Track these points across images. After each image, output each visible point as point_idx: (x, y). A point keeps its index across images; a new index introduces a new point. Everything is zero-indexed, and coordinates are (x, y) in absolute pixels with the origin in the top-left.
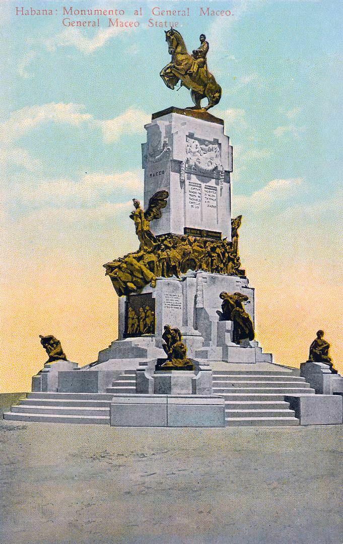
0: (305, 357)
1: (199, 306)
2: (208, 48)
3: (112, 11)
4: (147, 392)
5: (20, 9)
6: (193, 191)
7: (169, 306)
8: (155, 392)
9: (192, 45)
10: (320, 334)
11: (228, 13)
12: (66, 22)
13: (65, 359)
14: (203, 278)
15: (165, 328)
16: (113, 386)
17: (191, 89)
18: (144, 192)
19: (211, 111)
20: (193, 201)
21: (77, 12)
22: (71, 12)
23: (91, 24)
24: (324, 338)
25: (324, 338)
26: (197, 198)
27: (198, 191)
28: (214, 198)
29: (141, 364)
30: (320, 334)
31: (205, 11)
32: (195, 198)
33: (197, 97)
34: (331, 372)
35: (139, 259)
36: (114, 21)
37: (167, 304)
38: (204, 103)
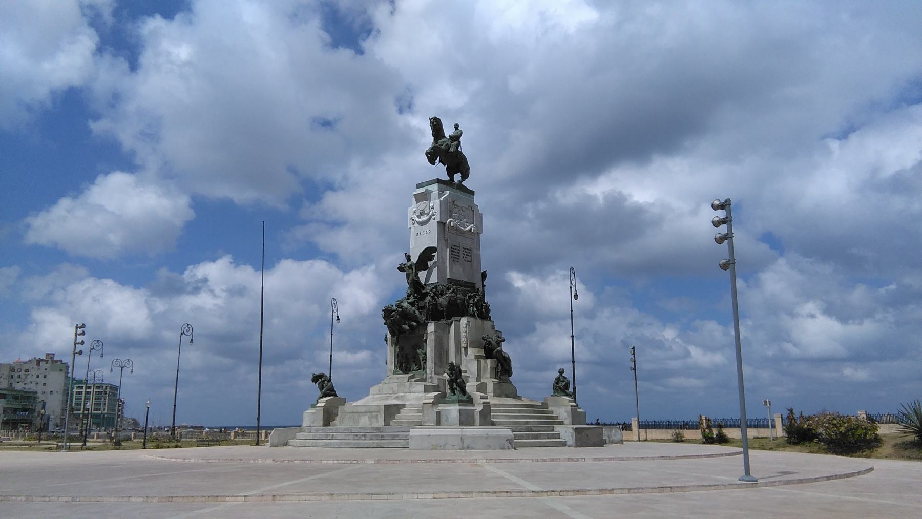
2: (462, 133)
9: (448, 131)
13: (335, 395)
15: (455, 394)
17: (446, 166)
20: (454, 256)
33: (450, 173)
35: (412, 304)
38: (457, 177)
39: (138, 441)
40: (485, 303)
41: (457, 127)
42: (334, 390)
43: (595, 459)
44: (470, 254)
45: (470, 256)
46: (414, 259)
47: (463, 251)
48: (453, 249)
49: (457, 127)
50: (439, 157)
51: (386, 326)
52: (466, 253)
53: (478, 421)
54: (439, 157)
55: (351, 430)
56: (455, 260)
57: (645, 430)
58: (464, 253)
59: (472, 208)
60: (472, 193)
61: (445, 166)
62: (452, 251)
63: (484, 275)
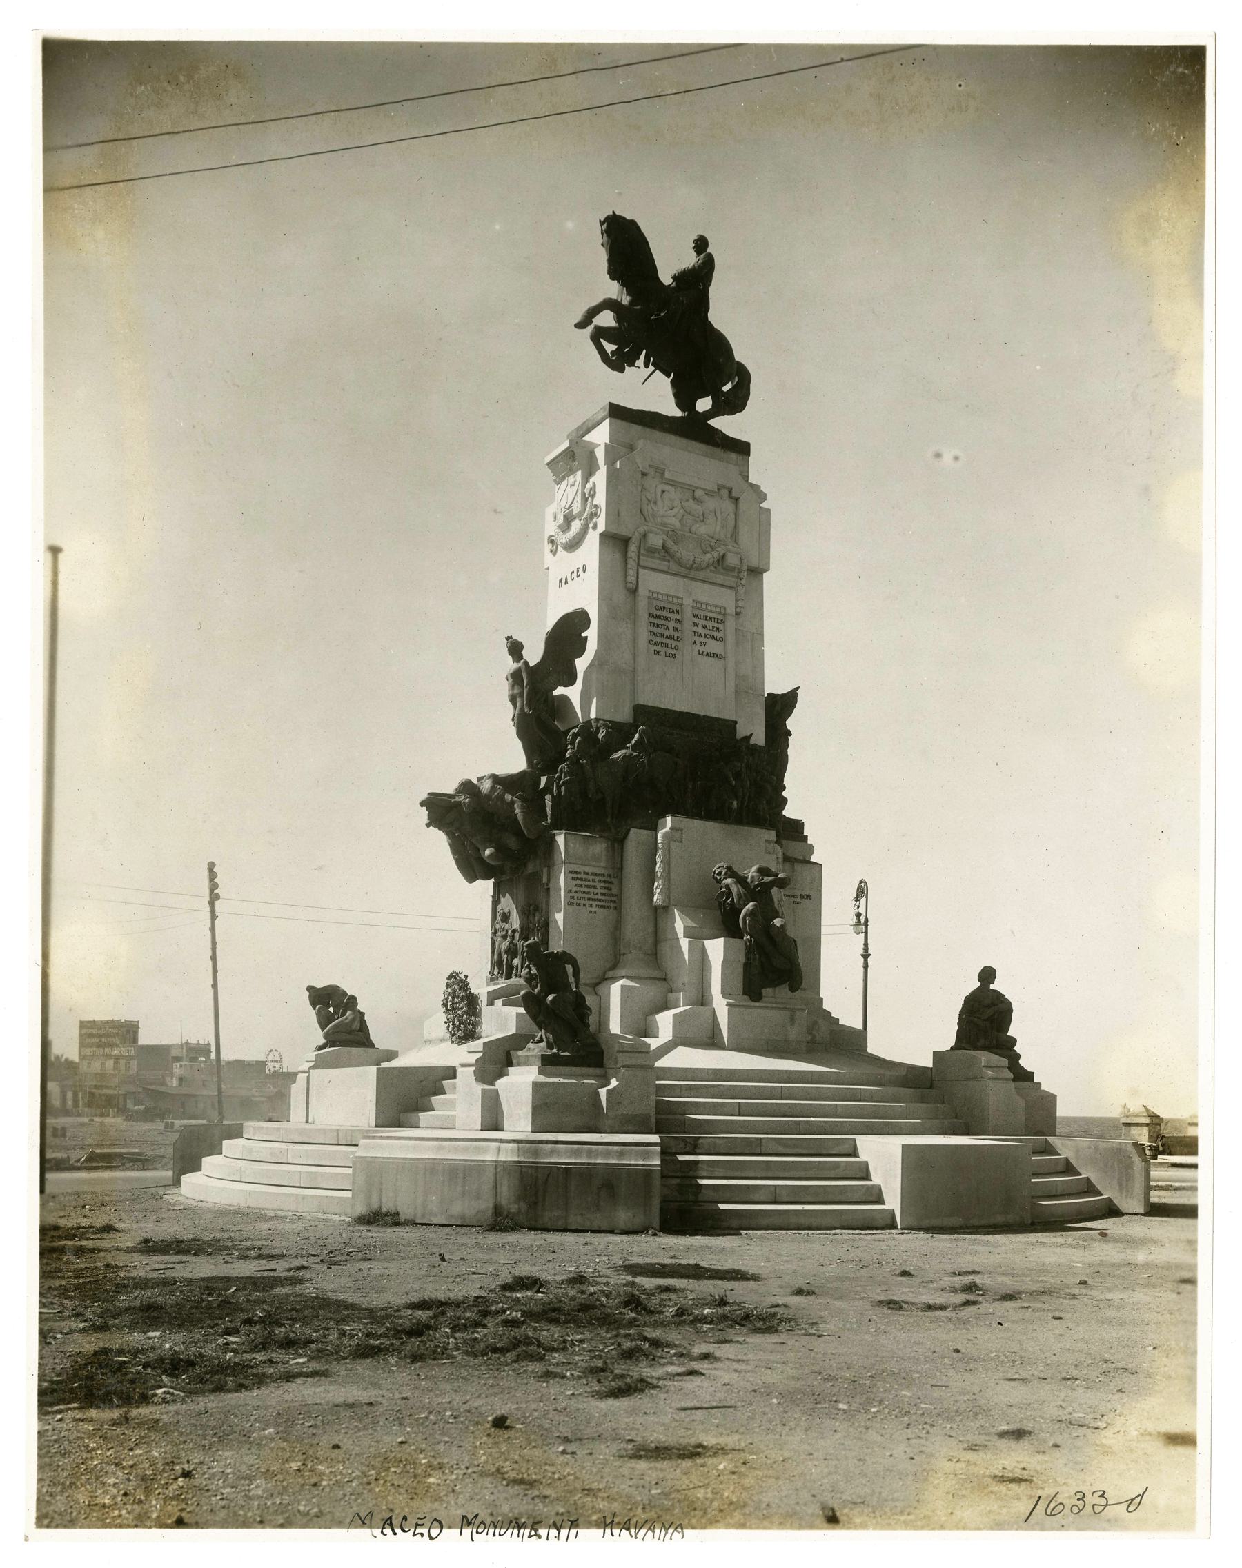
0: (946, 1038)
6: (659, 613)
7: (582, 902)
10: (987, 975)
14: (1060, 1318)
19: (717, 423)
20: (659, 640)
23: (705, 653)
26: (671, 632)
27: (674, 616)
28: (718, 635)
29: (986, 1440)
30: (987, 975)
32: (666, 633)
33: (684, 397)
34: (1012, 1076)
37: (576, 895)
39: (596, 1157)
40: (634, 727)
41: (701, 244)
42: (363, 1028)
43: (275, 1270)
44: (718, 635)
45: (721, 639)
46: (534, 654)
47: (695, 624)
48: (658, 617)
49: (701, 244)
50: (644, 351)
51: (789, 812)
52: (703, 632)
53: (659, 1116)
54: (644, 351)
55: (351, 1141)
56: (663, 650)
57: (481, 1049)
58: (700, 630)
59: (730, 491)
60: (742, 448)
61: (668, 376)
62: (654, 625)
63: (780, 706)
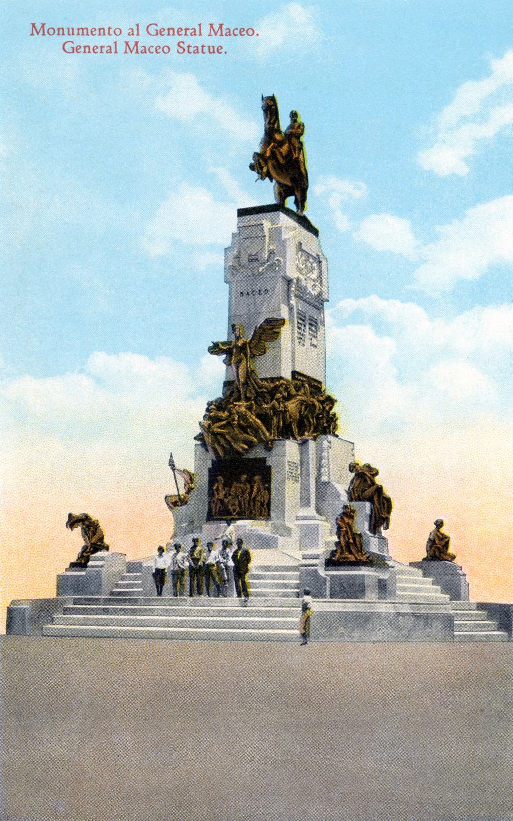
1: (324, 479)
3: (63, 29)
4: (325, 597)
5: (216, 27)
8: (331, 597)
9: (285, 123)
10: (439, 524)
11: (250, 32)
12: (68, 47)
16: (75, 604)
18: (229, 317)
21: (51, 31)
22: (43, 31)
24: (443, 530)
25: (443, 530)
30: (439, 524)
31: (216, 29)
36: (132, 45)
